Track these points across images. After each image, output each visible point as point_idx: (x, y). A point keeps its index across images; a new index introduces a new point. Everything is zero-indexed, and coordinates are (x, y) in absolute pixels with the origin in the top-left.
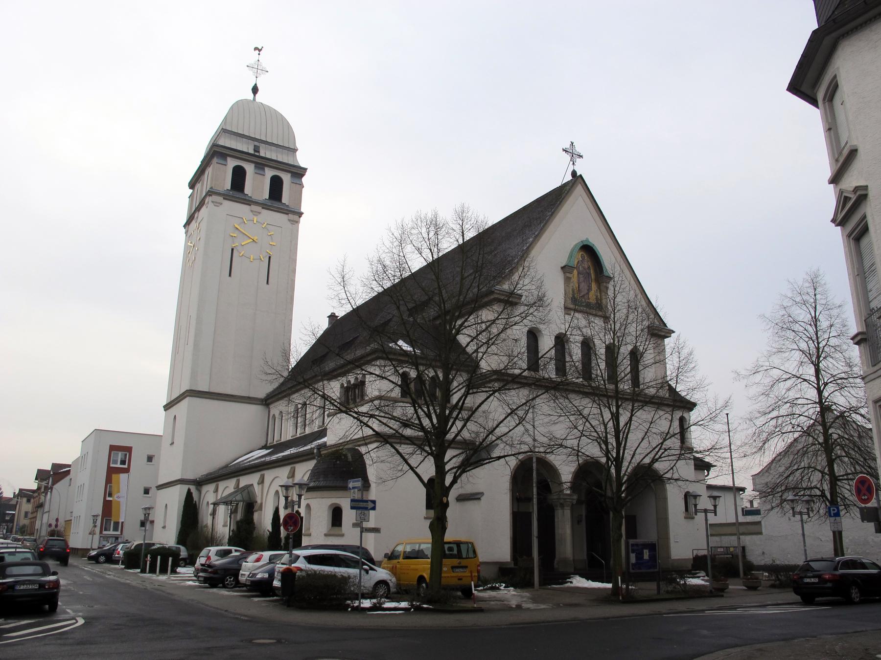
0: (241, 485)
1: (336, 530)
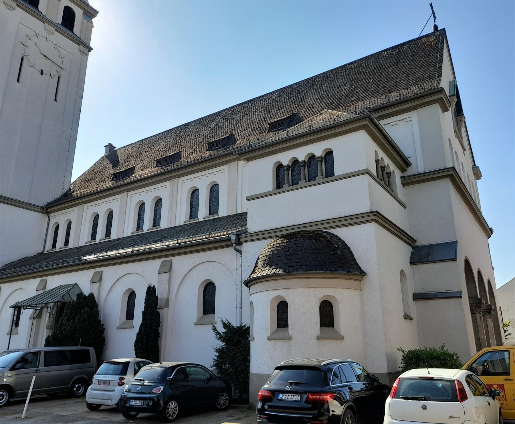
0: (49, 287)
1: (282, 333)
